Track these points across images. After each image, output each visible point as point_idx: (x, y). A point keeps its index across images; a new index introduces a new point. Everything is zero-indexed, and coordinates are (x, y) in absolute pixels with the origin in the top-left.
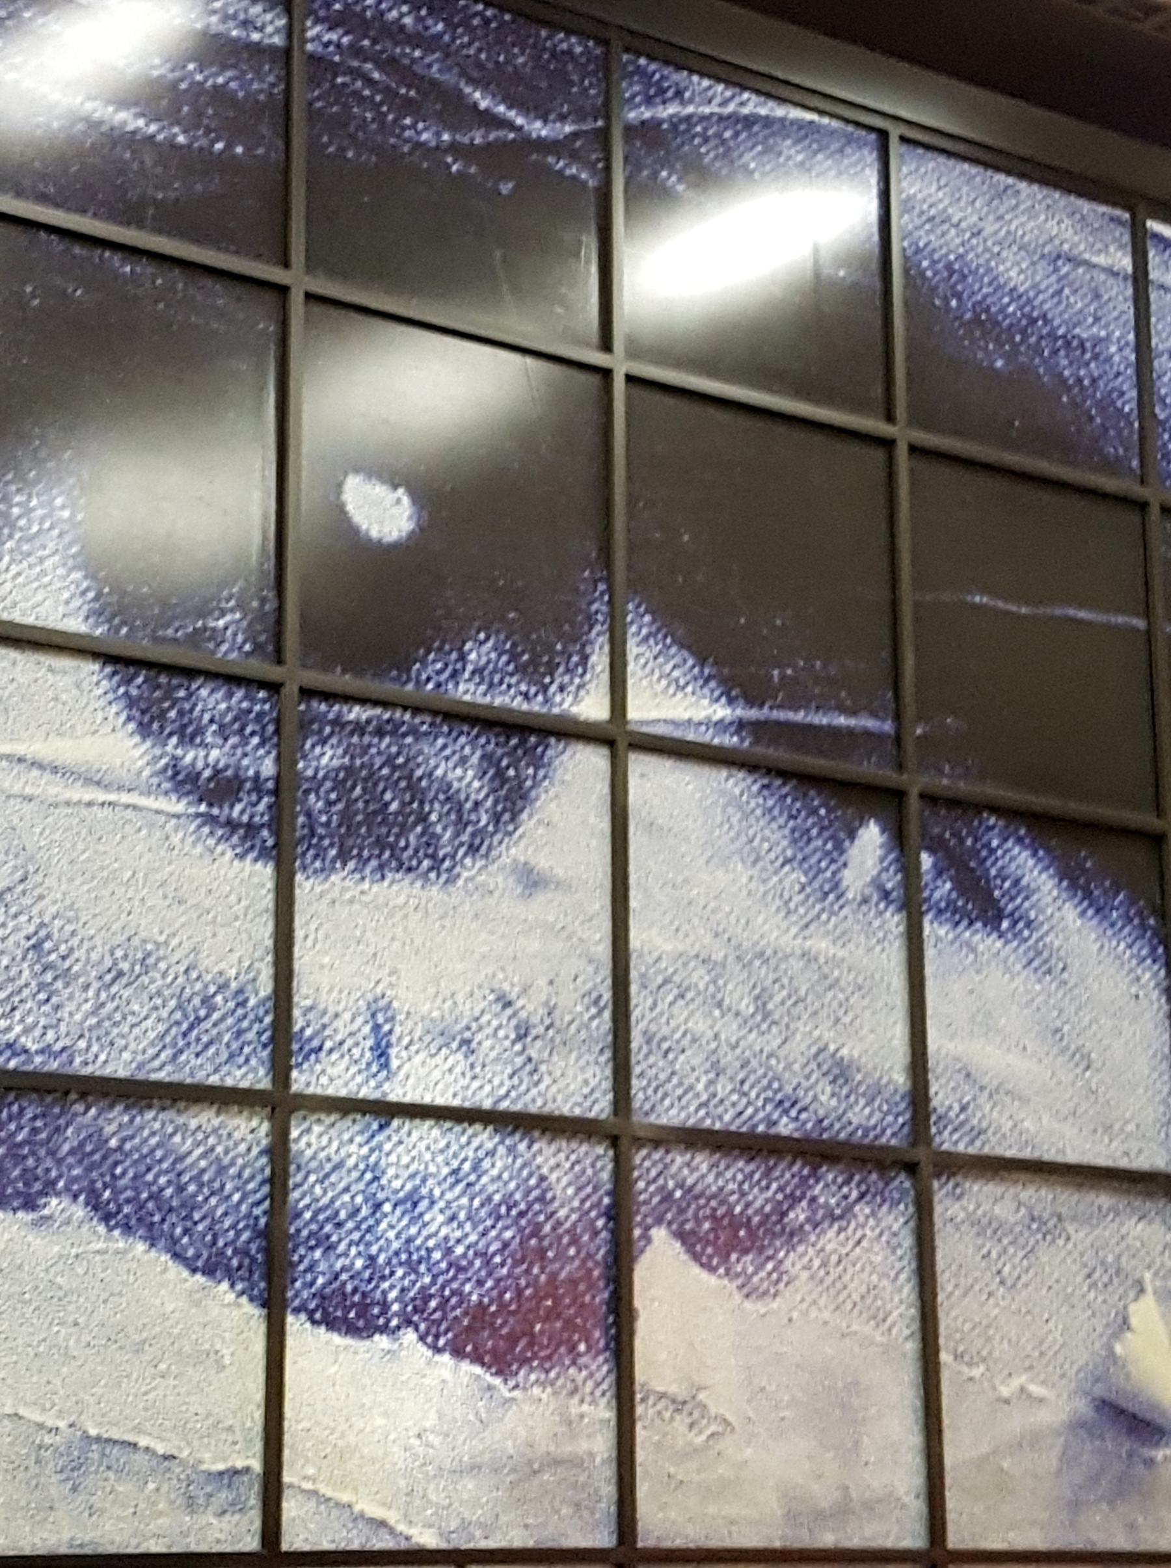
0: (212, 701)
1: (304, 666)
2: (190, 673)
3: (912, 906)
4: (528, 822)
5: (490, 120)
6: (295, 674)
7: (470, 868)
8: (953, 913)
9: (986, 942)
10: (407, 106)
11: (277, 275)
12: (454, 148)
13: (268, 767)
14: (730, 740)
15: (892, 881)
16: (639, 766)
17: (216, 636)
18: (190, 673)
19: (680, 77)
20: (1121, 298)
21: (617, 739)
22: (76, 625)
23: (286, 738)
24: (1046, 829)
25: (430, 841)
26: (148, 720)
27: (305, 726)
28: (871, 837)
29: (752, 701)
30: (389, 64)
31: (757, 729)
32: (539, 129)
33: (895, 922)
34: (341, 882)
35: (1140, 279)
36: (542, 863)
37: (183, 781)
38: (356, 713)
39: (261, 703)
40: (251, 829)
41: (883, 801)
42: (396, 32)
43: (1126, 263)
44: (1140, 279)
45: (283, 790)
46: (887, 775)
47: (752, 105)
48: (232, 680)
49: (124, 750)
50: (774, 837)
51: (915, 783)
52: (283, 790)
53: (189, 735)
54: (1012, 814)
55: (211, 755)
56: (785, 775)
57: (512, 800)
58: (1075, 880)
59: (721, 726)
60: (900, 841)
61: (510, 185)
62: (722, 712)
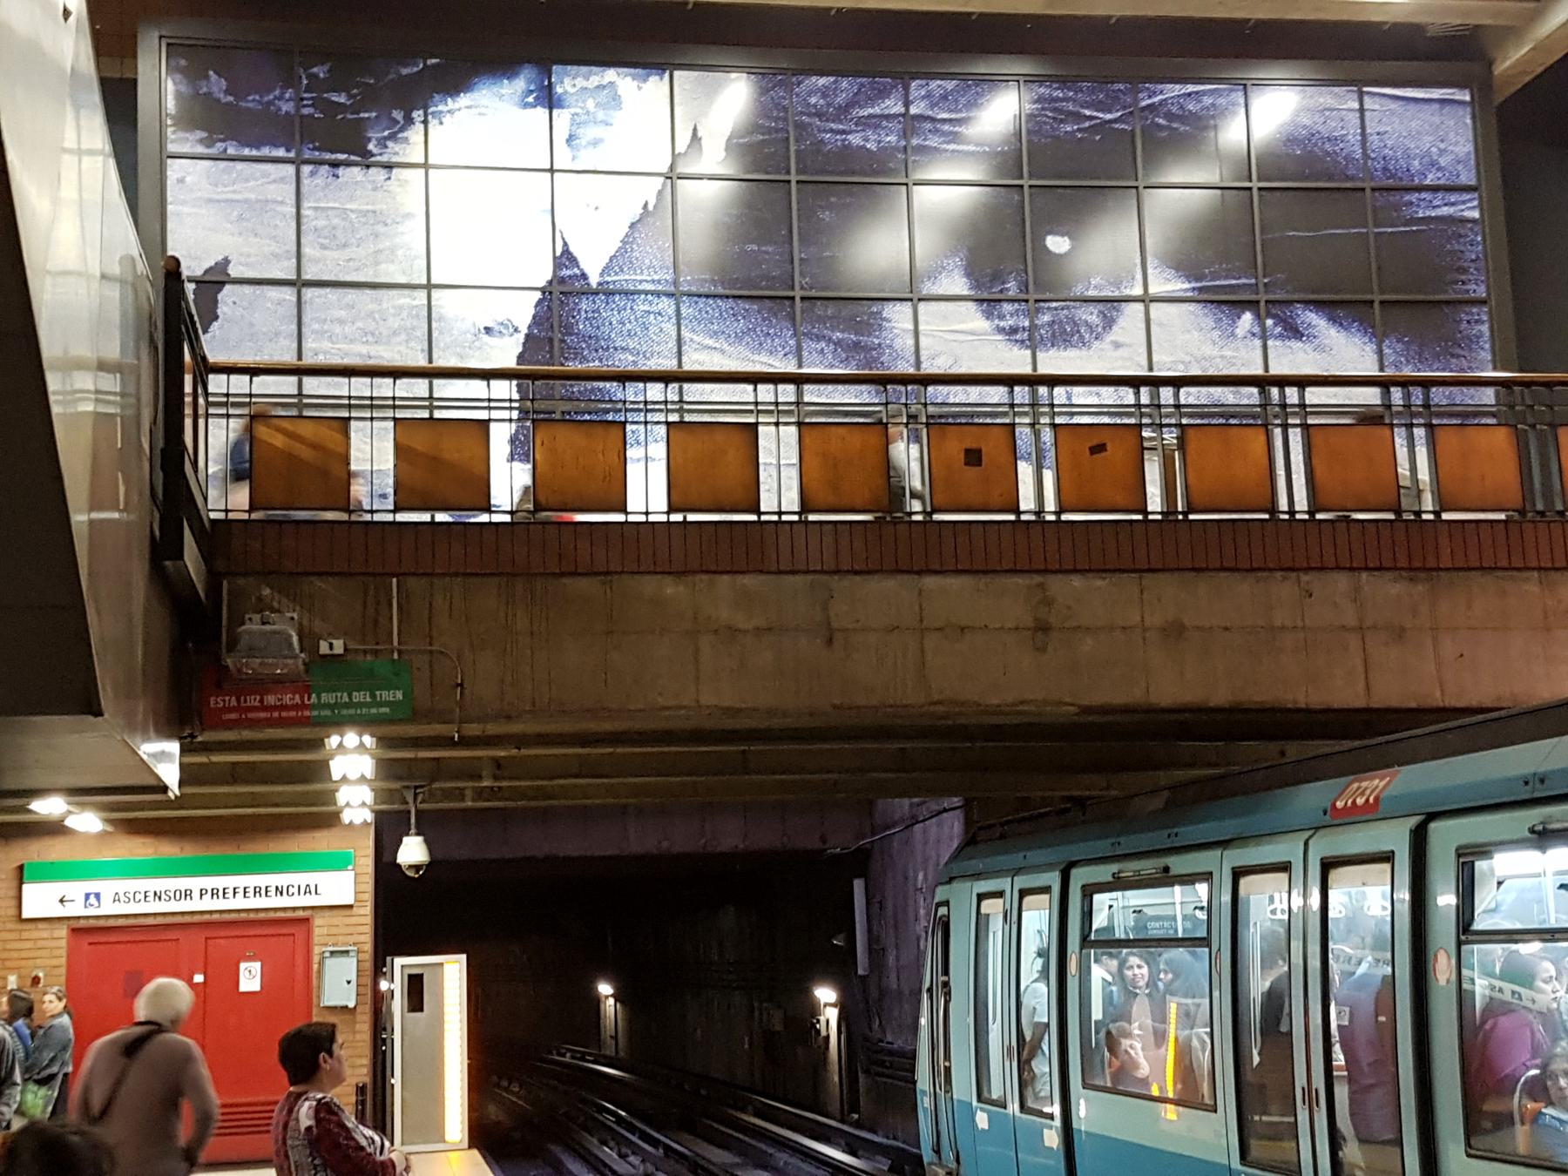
0: (1007, 307)
1: (334, 1026)
2: (1000, 301)
3: (1264, 338)
4: (1115, 328)
5: (1091, 118)
6: (1032, 296)
7: (1096, 344)
8: (1280, 336)
9: (1296, 345)
10: (1062, 121)
11: (791, 294)
12: (1079, 130)
13: (1027, 324)
14: (1190, 294)
15: (1257, 330)
16: (1154, 307)
17: (1008, 289)
18: (1000, 301)
19: (1160, 87)
20: (1354, 119)
21: (1146, 300)
22: (966, 293)
23: (1032, 315)
24: (1318, 305)
25: (1081, 337)
26: (989, 315)
27: (1038, 310)
28: (1247, 317)
29: (1197, 280)
30: (1055, 110)
31: (1200, 289)
32: (1109, 116)
33: (1258, 343)
34: (1053, 352)
35: (1362, 110)
36: (1121, 339)
37: (1001, 330)
38: (1054, 304)
39: (1023, 306)
40: (1023, 342)
41: (1252, 305)
42: (1058, 100)
43: (1356, 105)
44: (1362, 110)
45: (1033, 328)
46: (1253, 297)
47: (1191, 88)
48: (1012, 301)
49: (982, 324)
50: (1209, 322)
51: (1263, 297)
52: (1033, 328)
53: (1001, 317)
54: (1306, 303)
55: (1008, 323)
56: (1212, 302)
57: (1109, 323)
58: (1333, 320)
59: (1186, 290)
60: (1258, 317)
61: (167, 563)
62: (1187, 286)
